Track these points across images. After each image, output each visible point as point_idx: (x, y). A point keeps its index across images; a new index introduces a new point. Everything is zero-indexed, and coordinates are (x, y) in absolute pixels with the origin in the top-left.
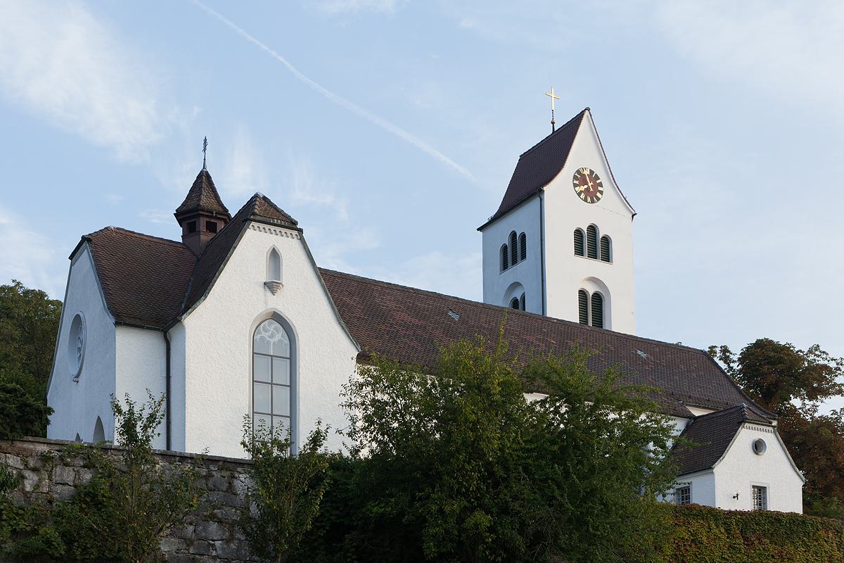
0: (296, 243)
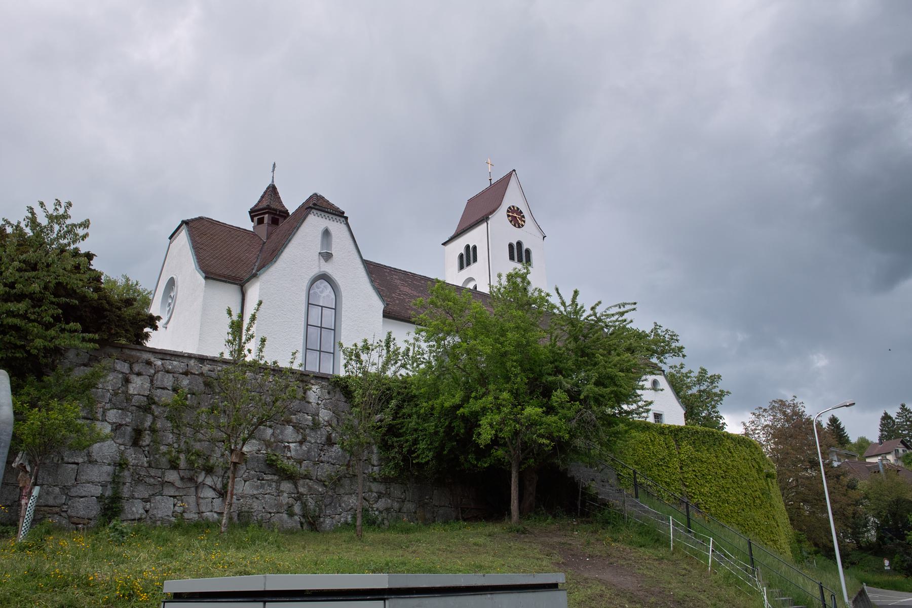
0: (343, 227)
